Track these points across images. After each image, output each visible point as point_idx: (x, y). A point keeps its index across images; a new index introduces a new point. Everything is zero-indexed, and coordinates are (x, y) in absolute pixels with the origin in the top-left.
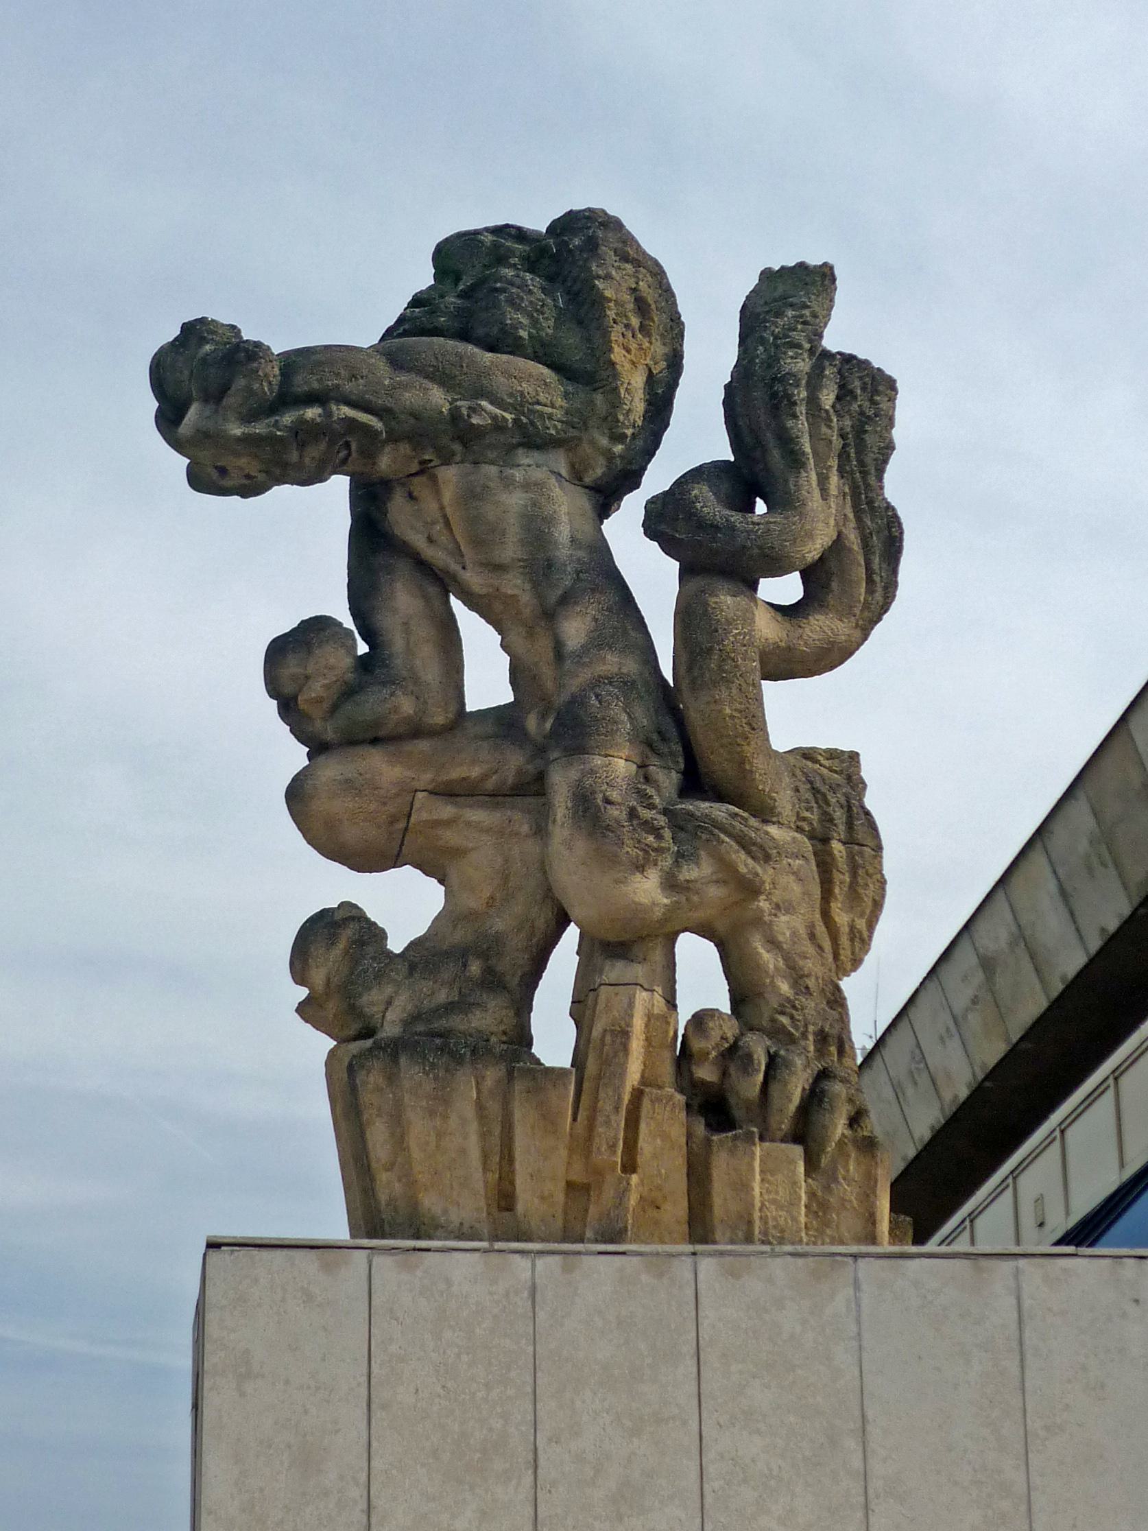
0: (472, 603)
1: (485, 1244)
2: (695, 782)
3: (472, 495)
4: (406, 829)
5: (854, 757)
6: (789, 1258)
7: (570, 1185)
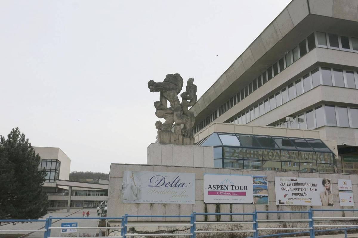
0: (168, 100)
2: (183, 114)
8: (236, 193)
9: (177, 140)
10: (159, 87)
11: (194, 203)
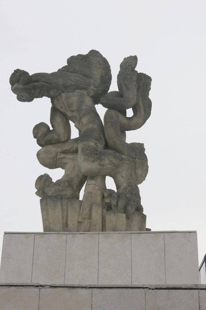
1: (57, 233)
2: (107, 146)
3: (67, 98)
4: (56, 160)
5: (143, 144)
6: (118, 234)
7: (79, 222)
9: (84, 219)
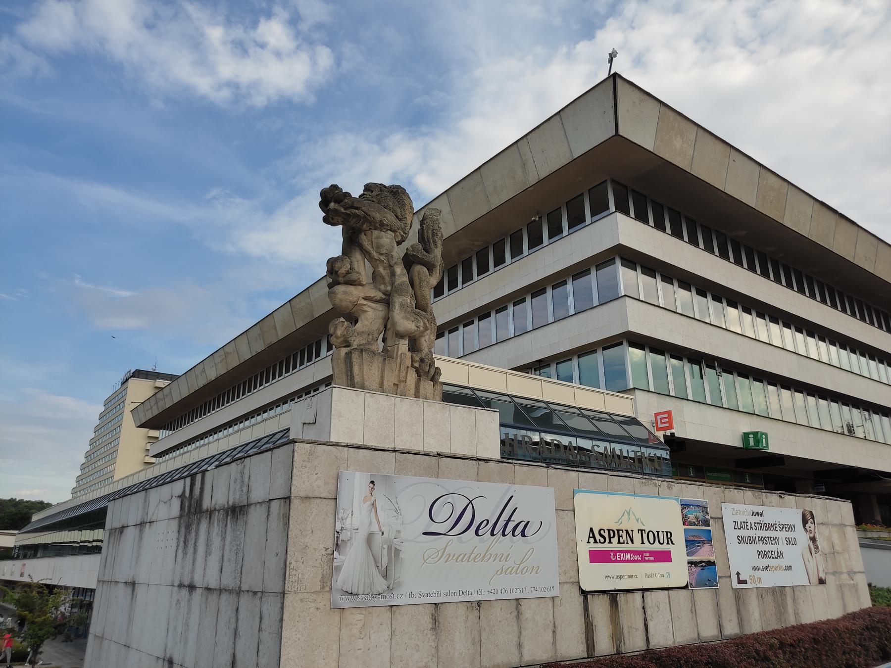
8: (652, 553)
10: (354, 211)
11: (555, 593)
